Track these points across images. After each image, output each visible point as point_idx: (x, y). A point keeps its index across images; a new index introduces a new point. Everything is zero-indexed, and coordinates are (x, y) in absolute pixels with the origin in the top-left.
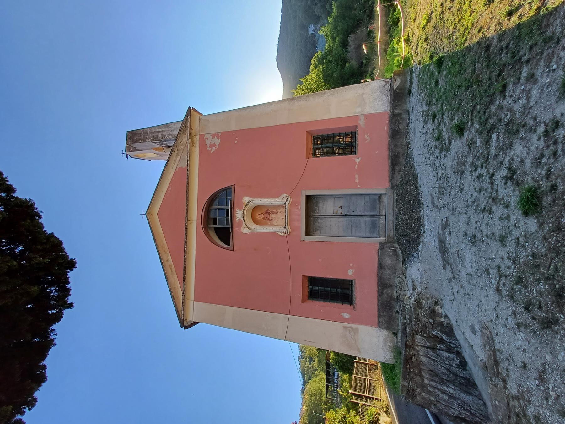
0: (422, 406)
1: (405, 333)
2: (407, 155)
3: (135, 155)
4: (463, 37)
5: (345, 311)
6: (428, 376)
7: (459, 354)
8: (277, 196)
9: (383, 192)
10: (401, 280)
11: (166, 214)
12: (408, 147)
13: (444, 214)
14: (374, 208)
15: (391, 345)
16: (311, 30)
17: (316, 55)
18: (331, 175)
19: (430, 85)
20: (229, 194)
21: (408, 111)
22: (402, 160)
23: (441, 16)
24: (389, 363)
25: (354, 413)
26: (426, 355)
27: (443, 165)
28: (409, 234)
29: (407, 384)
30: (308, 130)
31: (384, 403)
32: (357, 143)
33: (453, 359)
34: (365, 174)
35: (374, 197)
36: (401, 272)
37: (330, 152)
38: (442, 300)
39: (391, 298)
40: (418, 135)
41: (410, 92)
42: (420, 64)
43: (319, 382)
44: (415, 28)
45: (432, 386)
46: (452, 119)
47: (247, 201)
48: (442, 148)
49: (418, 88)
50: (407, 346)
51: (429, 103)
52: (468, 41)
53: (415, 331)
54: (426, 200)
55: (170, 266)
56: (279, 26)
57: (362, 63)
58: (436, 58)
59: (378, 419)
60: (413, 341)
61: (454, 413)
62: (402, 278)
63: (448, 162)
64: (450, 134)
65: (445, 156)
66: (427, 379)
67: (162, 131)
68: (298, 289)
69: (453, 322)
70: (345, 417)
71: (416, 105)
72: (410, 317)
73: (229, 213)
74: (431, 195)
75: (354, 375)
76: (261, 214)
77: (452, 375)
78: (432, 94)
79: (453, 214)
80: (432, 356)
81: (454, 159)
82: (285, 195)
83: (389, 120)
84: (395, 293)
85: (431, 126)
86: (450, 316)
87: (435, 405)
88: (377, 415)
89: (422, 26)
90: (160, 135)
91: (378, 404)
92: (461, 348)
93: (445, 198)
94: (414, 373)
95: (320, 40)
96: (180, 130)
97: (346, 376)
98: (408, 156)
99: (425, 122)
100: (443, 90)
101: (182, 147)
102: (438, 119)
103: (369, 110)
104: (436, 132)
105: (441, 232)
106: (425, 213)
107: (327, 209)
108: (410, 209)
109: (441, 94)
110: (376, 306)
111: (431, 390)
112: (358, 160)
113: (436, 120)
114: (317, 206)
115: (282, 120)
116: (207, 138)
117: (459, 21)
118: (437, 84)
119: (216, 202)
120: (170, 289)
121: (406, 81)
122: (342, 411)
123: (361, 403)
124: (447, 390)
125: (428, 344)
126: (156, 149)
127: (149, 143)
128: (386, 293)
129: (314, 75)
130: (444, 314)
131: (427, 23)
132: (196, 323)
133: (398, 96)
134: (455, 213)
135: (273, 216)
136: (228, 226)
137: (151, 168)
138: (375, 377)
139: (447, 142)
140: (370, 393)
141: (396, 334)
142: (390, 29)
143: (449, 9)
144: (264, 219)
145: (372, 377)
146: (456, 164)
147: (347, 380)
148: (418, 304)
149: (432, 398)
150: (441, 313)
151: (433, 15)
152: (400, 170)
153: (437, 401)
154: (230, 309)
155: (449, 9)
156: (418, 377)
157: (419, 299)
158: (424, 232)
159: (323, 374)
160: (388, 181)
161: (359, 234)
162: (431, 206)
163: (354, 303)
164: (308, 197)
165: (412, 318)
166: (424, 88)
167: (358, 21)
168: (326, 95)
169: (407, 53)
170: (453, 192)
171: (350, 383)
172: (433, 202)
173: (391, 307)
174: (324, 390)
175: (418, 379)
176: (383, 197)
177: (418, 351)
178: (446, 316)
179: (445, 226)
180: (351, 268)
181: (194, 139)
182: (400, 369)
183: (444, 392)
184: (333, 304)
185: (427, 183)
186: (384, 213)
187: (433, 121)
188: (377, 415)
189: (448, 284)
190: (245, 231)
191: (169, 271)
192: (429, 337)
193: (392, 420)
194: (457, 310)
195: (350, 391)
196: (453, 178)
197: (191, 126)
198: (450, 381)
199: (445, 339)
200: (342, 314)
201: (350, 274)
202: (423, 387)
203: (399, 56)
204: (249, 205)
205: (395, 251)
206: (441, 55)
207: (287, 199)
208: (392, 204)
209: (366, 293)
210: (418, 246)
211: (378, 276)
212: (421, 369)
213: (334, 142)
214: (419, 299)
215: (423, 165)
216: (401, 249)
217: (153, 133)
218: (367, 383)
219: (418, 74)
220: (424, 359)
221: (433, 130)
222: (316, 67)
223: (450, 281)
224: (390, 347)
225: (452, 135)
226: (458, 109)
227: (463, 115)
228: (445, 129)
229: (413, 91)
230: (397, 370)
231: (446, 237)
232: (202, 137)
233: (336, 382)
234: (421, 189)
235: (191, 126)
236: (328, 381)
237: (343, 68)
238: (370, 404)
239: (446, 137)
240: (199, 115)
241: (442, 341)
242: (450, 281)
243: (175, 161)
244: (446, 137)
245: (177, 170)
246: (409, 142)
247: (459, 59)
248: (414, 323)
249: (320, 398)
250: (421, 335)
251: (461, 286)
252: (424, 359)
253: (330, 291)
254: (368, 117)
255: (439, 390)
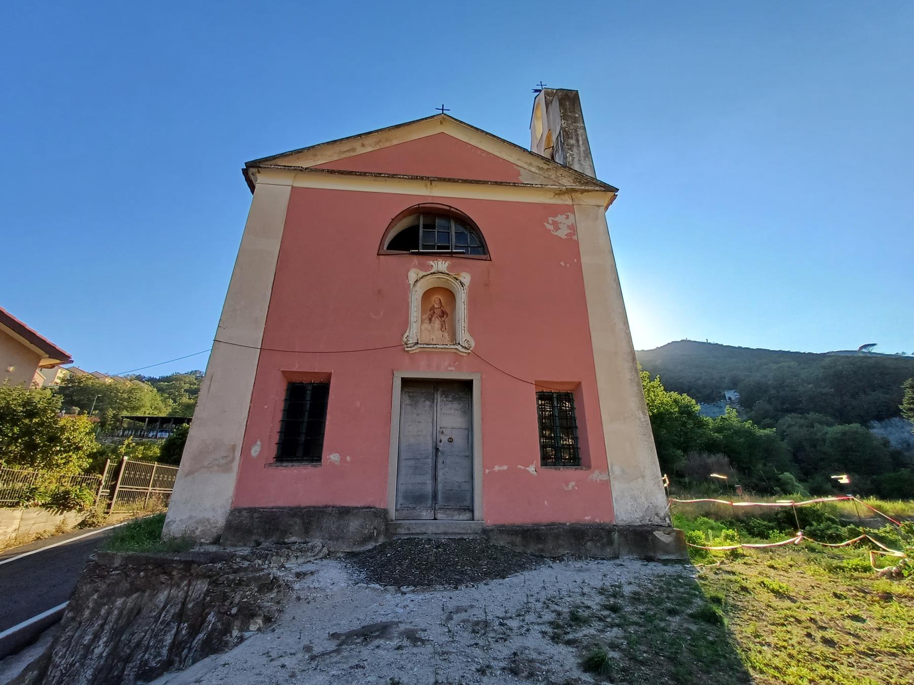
0: (73, 594)
1: (213, 561)
2: (542, 556)
3: (539, 103)
4: (766, 665)
5: (264, 447)
6: (129, 605)
7: (167, 666)
8: (471, 331)
9: (477, 514)
10: (317, 550)
11: (441, 148)
12: (554, 559)
13: (436, 634)
14: (448, 498)
15: (198, 532)
16: (730, 394)
17: (694, 401)
18: (507, 426)
19: (668, 598)
20: (475, 250)
21: (617, 557)
22: (532, 548)
23: (792, 619)
24: (165, 530)
25: (86, 465)
26: (170, 601)
27: (528, 630)
28: (400, 564)
29: (116, 565)
30: (583, 384)
31: (100, 519)
32: (562, 468)
33: (159, 654)
34: (509, 484)
35: (468, 498)
36: (331, 549)
37: (545, 424)
38: (273, 630)
39: (285, 532)
40: (579, 578)
41: (649, 559)
42: (700, 577)
43: (151, 404)
44: (759, 569)
45: (109, 613)
46: (613, 646)
47: (465, 278)
48: (558, 626)
49: (658, 576)
50: (188, 564)
51: (636, 598)
52: (761, 676)
53: (217, 580)
54: (463, 595)
55: (354, 150)
56: (736, 344)
57: (683, 476)
58: (720, 612)
59: (70, 509)
60: (198, 577)
61: (56, 654)
62: (320, 551)
63: (535, 643)
64: (585, 643)
65: (544, 633)
66: (125, 603)
67: (579, 146)
68: (308, 366)
69: (224, 658)
70: (78, 448)
71: (629, 573)
72: (245, 570)
73: (444, 251)
74: (472, 607)
75: (156, 464)
76: (440, 304)
77: (128, 651)
78: (653, 604)
79: (435, 653)
80: (168, 611)
81: (540, 653)
82: (473, 344)
83: (600, 524)
84: (293, 539)
85: (595, 602)
86: (241, 647)
87: (73, 619)
88: (78, 507)
89: (767, 581)
90: (572, 142)
91: (100, 509)
92: (179, 669)
93: (465, 634)
94: (136, 577)
95: (716, 410)
96: (581, 174)
97: (158, 451)
98: (539, 559)
99: (602, 591)
100: (663, 624)
101: (553, 177)
102: (609, 616)
103: (617, 488)
104: (587, 613)
105: (402, 627)
106: (438, 595)
107: (448, 416)
108: (447, 565)
109: (657, 622)
110: (271, 505)
111: (103, 611)
112: (531, 469)
113: (606, 613)
114: (454, 399)
115: (598, 341)
116: (567, 217)
117: (791, 656)
118: (672, 612)
119: (461, 229)
120: (313, 147)
121: (668, 553)
122: (91, 445)
123: (104, 478)
124: (101, 642)
125: (190, 606)
126: (549, 137)
127: (558, 124)
128: (296, 523)
129: (665, 398)
130: (247, 634)
131: (773, 591)
132: (252, 187)
133: (640, 540)
134: (437, 657)
135: (437, 323)
136: (420, 245)
137: (521, 126)
138: (152, 502)
139: (570, 636)
140: (122, 495)
141: (216, 541)
142: (742, 522)
143: (809, 635)
144: (433, 308)
145: (151, 497)
146: (530, 657)
147: (151, 454)
148: (270, 584)
149: (87, 613)
150: (248, 630)
151: (788, 603)
152: (513, 544)
153: (80, 623)
154: (274, 246)
155: (809, 635)
156: (128, 585)
157: (279, 586)
158: (404, 593)
159: (169, 410)
160: (496, 523)
161: (403, 471)
162: (451, 605)
163: (278, 464)
164: (467, 386)
165: (242, 574)
166: (661, 587)
167: (749, 468)
168: (641, 415)
169: (714, 553)
170: (477, 652)
171: (142, 459)
172: (459, 610)
173: (267, 534)
174: (139, 414)
175: (125, 585)
176: (468, 515)
177: (178, 585)
178: (241, 639)
179: (413, 637)
180: (343, 460)
181: (566, 197)
182: (148, 551)
183: (97, 636)
184: (277, 427)
185: (494, 597)
186: (439, 516)
187: (606, 607)
188: (78, 507)
189: (301, 646)
190: (413, 275)
191: (345, 147)
192: (203, 607)
193: (68, 533)
194: (249, 664)
195: (126, 458)
196: (503, 651)
197: (588, 191)
198: (116, 647)
199: (198, 638)
200: (259, 443)
201: (331, 457)
202: (108, 596)
203: (707, 539)
204: (457, 284)
205: (369, 538)
206: (726, 621)
207: (465, 348)
208: (457, 530)
209: (297, 486)
210: (379, 580)
211: (326, 507)
212: (144, 591)
213: (562, 429)
214: (279, 586)
215: (525, 589)
216: (375, 548)
217: (576, 131)
218: (141, 489)
219: (684, 574)
220: (162, 597)
221: (588, 607)
222: (675, 401)
223: (308, 649)
224: (194, 532)
225: (586, 648)
226: (633, 659)
227: (624, 670)
228: (592, 631)
229: (652, 565)
230: (148, 544)
231: (391, 639)
232: (570, 209)
233: (151, 435)
234: (481, 585)
235: (588, 191)
236: (153, 420)
237: (675, 445)
238: (100, 493)
239: (579, 635)
240: (605, 204)
241: (194, 631)
242: (308, 649)
243: (530, 164)
244: (579, 635)
245: (516, 167)
246: (563, 560)
247: (725, 657)
248: (231, 577)
249: (126, 408)
250: (207, 593)
251: (293, 675)
252: (162, 597)
253: (301, 422)
254: (606, 486)
255: (102, 626)
